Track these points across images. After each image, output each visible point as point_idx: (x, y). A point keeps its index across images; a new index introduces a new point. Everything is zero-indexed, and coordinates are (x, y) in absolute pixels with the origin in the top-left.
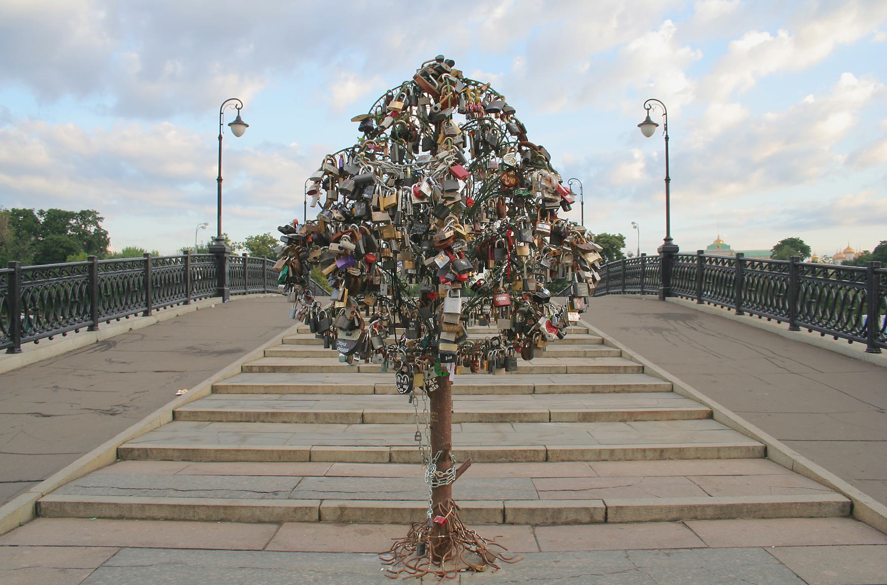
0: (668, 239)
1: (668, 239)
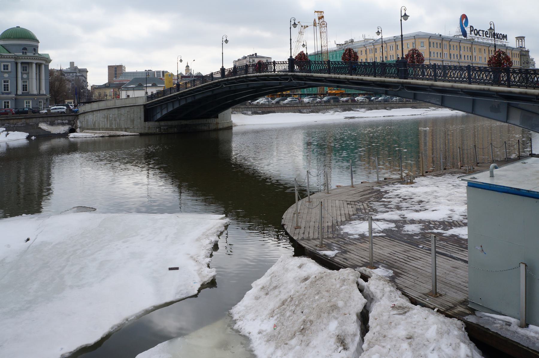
0: (223, 67)
1: (223, 67)
